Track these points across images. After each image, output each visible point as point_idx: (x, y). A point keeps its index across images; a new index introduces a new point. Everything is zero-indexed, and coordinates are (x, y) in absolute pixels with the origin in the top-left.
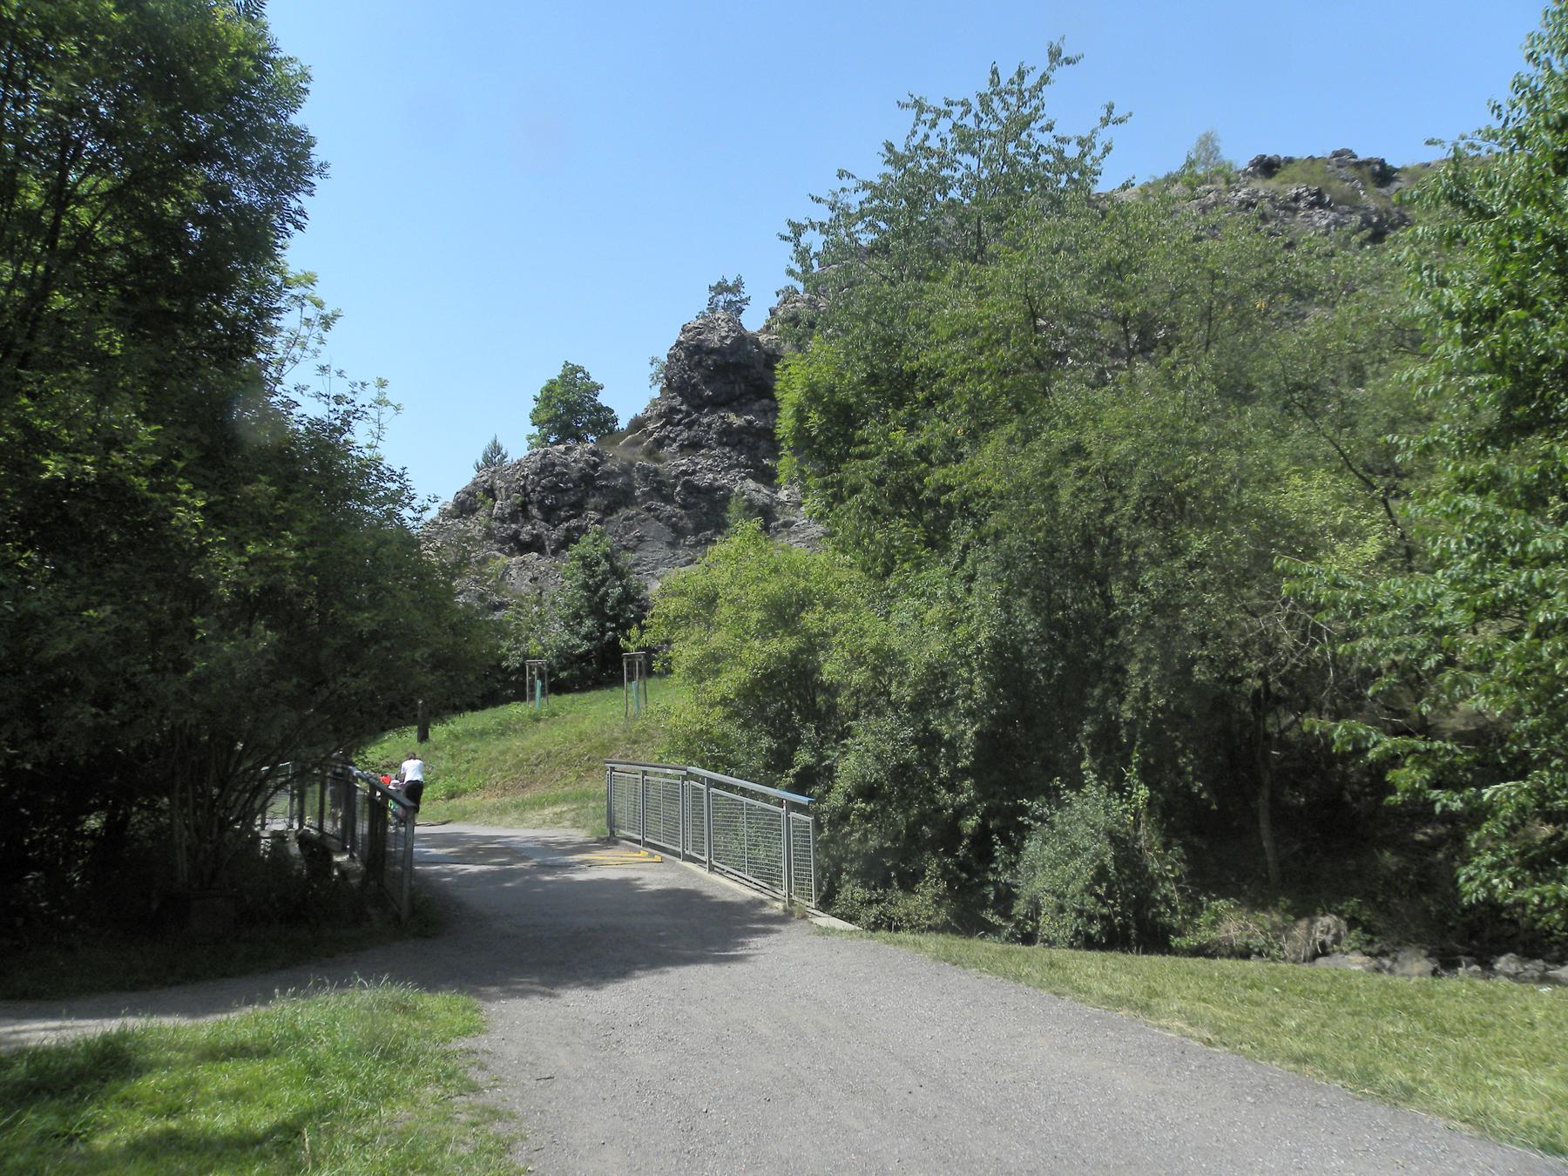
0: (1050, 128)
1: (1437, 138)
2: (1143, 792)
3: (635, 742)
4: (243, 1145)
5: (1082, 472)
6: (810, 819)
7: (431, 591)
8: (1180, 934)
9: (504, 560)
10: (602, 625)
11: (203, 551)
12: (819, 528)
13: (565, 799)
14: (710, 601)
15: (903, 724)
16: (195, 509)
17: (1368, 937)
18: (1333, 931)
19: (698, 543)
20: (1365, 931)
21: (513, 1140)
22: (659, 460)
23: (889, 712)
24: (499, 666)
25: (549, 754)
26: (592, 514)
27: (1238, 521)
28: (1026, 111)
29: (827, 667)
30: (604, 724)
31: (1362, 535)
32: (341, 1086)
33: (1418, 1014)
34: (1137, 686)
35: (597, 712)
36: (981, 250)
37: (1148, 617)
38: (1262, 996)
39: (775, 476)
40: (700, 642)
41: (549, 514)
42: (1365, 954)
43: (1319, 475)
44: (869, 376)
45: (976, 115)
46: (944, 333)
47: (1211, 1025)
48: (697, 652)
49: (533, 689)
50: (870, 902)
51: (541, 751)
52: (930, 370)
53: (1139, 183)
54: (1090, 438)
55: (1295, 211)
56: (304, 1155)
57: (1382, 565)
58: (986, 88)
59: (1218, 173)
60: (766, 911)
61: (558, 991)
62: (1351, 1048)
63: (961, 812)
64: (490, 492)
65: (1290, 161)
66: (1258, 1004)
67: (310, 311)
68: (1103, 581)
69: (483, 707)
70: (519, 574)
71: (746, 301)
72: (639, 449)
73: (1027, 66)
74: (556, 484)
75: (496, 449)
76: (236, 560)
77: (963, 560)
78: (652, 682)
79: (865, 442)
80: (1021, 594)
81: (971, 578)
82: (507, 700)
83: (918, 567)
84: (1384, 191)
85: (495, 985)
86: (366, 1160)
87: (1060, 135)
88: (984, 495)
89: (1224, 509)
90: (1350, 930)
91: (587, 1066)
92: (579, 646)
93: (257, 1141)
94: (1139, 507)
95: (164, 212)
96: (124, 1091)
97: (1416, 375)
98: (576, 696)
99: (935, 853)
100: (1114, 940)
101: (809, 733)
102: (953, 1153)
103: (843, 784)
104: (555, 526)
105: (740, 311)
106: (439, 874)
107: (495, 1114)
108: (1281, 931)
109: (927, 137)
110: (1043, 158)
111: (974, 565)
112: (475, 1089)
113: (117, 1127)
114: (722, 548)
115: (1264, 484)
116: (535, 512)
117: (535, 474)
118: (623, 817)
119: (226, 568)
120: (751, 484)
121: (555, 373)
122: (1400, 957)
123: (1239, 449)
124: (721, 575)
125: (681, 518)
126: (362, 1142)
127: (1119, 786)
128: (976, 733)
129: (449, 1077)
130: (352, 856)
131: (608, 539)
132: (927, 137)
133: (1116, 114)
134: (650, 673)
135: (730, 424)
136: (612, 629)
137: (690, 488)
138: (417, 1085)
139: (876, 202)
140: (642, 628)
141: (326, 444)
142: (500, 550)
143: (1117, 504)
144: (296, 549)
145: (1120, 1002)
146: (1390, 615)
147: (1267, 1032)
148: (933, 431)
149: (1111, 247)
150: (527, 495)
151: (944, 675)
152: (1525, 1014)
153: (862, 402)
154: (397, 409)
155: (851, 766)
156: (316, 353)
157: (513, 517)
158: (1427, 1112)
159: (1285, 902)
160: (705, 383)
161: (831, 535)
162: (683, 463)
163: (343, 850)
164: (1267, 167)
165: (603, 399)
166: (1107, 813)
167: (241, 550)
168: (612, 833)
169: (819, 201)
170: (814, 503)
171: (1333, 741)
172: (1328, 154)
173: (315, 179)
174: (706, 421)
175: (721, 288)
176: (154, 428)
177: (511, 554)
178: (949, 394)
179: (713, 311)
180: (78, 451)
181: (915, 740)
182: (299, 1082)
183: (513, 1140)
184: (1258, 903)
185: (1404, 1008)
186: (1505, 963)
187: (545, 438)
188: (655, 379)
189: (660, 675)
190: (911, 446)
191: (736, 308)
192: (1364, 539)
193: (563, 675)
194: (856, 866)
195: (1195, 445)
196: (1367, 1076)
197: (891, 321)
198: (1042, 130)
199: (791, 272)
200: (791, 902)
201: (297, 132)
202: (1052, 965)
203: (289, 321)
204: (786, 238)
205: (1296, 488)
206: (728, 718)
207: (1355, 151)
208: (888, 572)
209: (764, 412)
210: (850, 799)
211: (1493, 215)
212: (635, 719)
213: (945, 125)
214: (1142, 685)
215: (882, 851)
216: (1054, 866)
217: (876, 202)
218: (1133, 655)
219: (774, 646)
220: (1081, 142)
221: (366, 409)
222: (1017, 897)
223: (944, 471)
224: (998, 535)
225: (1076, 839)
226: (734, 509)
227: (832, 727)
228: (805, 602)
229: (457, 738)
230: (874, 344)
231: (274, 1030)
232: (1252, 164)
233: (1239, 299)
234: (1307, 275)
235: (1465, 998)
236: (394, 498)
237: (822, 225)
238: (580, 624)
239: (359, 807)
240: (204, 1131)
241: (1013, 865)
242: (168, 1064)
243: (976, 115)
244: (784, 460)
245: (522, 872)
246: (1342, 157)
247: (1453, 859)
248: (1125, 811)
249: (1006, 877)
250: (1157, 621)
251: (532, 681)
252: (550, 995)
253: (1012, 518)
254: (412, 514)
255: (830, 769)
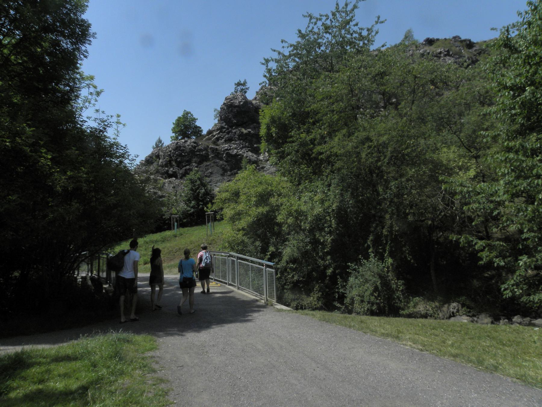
0: (357, 25)
1: (495, 27)
2: (390, 260)
4: (67, 395)
5: (369, 147)
6: (273, 270)
7: (137, 192)
8: (403, 310)
11: (52, 174)
14: (237, 194)
15: (306, 237)
16: (48, 159)
17: (469, 310)
18: (457, 308)
19: (232, 174)
20: (468, 308)
21: (169, 390)
22: (217, 145)
24: (161, 217)
26: (194, 164)
27: (424, 164)
28: (348, 18)
31: (468, 169)
32: (104, 371)
33: (493, 338)
36: (332, 69)
38: (437, 332)
39: (260, 150)
40: (234, 208)
41: (179, 165)
42: (468, 316)
43: (453, 148)
44: (293, 114)
45: (331, 20)
46: (320, 98)
47: (421, 344)
49: (174, 226)
50: (294, 300)
51: (177, 248)
52: (315, 111)
53: (388, 46)
54: (372, 134)
55: (440, 57)
56: (89, 399)
57: (477, 179)
58: (334, 10)
59: (413, 44)
60: (258, 303)
61: (184, 334)
62: (472, 351)
63: (326, 267)
64: (158, 157)
65: (438, 40)
66: (436, 336)
67: (92, 90)
70: (169, 186)
71: (248, 89)
72: (210, 141)
73: (349, 1)
76: (63, 177)
78: (216, 223)
82: (165, 230)
83: (311, 182)
84: (470, 50)
85: (162, 331)
86: (113, 400)
87: (360, 27)
89: (419, 160)
90: (462, 308)
91: (195, 361)
93: (71, 393)
94: (391, 159)
95: (36, 51)
96: (23, 374)
97: (492, 110)
98: (189, 228)
99: (316, 282)
100: (379, 312)
102: (332, 393)
103: (285, 258)
104: (181, 169)
105: (246, 92)
107: (162, 381)
108: (439, 308)
109: (313, 28)
110: (354, 35)
111: (331, 180)
112: (154, 371)
113: (20, 388)
114: (241, 175)
115: (434, 151)
116: (174, 163)
117: (174, 150)
119: (61, 180)
120: (250, 154)
121: (180, 114)
122: (480, 317)
123: (425, 139)
124: (241, 185)
125: (226, 166)
126: (112, 393)
127: (382, 259)
128: (331, 240)
129: (145, 367)
130: (110, 285)
131: (200, 173)
132: (313, 28)
133: (381, 20)
134: (215, 220)
135: (242, 133)
137: (229, 155)
138: (132, 370)
139: (295, 51)
140: (213, 204)
141: (97, 136)
142: (162, 177)
143: (382, 158)
144: (86, 174)
145: (388, 335)
146: (481, 196)
147: (442, 346)
148: (316, 133)
149: (379, 67)
150: (171, 157)
151: (321, 220)
152: (531, 338)
153: (290, 123)
154: (124, 125)
155: (288, 251)
156: (94, 105)
157: (166, 165)
158: (504, 375)
159: (439, 298)
160: (234, 118)
162: (226, 146)
163: (106, 283)
164: (430, 42)
165: (198, 124)
166: (378, 268)
167: (65, 173)
169: (274, 51)
170: (274, 159)
171: (460, 243)
172: (451, 37)
173: (91, 39)
174: (234, 131)
175: (239, 84)
176: (32, 129)
177: (165, 178)
178: (321, 120)
179: (236, 92)
180: (4, 138)
181: (310, 242)
182: (88, 370)
183: (169, 390)
184: (431, 299)
185: (488, 336)
186: (516, 319)
187: (177, 138)
190: (308, 139)
191: (244, 91)
192: (469, 170)
193: (185, 221)
195: (409, 137)
196: (480, 362)
197: (301, 93)
198: (354, 25)
200: (267, 300)
201: (83, 21)
202: (362, 322)
203: (84, 92)
204: (263, 64)
205: (445, 153)
207: (461, 36)
208: (299, 184)
209: (254, 128)
210: (287, 263)
211: (521, 51)
212: (211, 236)
213: (319, 23)
214: (391, 224)
215: (298, 281)
217: (295, 51)
219: (261, 210)
220: (368, 30)
222: (346, 297)
224: (339, 170)
228: (270, 194)
229: (147, 243)
231: (80, 350)
232: (425, 41)
233: (423, 85)
234: (448, 77)
235: (509, 332)
236: (123, 156)
237: (276, 59)
238: (190, 203)
240: (52, 389)
241: (345, 286)
242: (39, 364)
243: (331, 20)
245: (172, 290)
246: (456, 39)
247: (498, 282)
248: (384, 267)
249: (341, 290)
250: (396, 200)
252: (182, 335)
254: (129, 162)
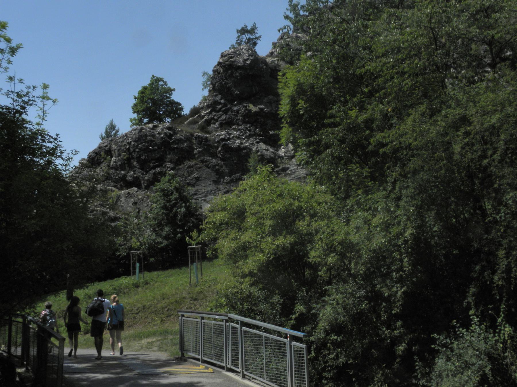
3: (195, 300)
5: (467, 134)
6: (304, 346)
9: (116, 192)
10: (175, 230)
12: (302, 172)
13: (154, 334)
15: (359, 288)
19: (232, 181)
22: (208, 132)
23: (351, 280)
24: (114, 254)
25: (144, 307)
26: (169, 164)
29: (313, 254)
30: (177, 289)
34: (503, 264)
35: (174, 282)
37: (509, 222)
40: (235, 239)
41: (144, 166)
48: (233, 245)
49: (134, 268)
51: (140, 305)
63: (395, 341)
68: (478, 199)
69: (105, 280)
70: (126, 199)
71: (258, 38)
72: (196, 126)
74: (148, 147)
75: (112, 127)
77: (394, 188)
78: (205, 264)
79: (333, 116)
80: (429, 209)
81: (399, 199)
82: (119, 276)
88: (406, 149)
92: (162, 243)
98: (160, 273)
101: (302, 293)
103: (323, 324)
104: (147, 172)
105: (255, 44)
106: (79, 380)
111: (401, 189)
116: (135, 163)
117: (135, 141)
118: (189, 343)
120: (262, 146)
121: (146, 82)
124: (247, 199)
125: (222, 167)
128: (403, 293)
130: (27, 369)
131: (178, 179)
135: (250, 111)
136: (180, 233)
137: (227, 149)
140: (200, 231)
142: (115, 186)
143: (490, 153)
148: (376, 109)
150: (130, 154)
151: (384, 258)
154: (54, 101)
155: (327, 313)
156: (6, 69)
157: (122, 167)
161: (312, 175)
162: (223, 133)
165: (175, 97)
166: (486, 343)
168: (183, 354)
170: (302, 155)
175: (243, 31)
177: (121, 189)
179: (239, 44)
181: (366, 298)
187: (140, 121)
188: (205, 86)
189: (210, 259)
190: (361, 119)
191: (252, 43)
193: (152, 260)
194: (330, 375)
197: (348, 44)
199: (287, 17)
206: (252, 285)
215: (346, 365)
216: (454, 376)
218: (501, 245)
219: (280, 241)
221: (36, 99)
223: (382, 134)
224: (415, 172)
225: (467, 358)
226: (252, 162)
227: (317, 289)
230: (337, 59)
236: (52, 152)
238: (162, 230)
239: (32, 339)
241: (428, 374)
244: (284, 130)
245: (130, 379)
251: (134, 264)
253: (424, 161)
255: (315, 316)
